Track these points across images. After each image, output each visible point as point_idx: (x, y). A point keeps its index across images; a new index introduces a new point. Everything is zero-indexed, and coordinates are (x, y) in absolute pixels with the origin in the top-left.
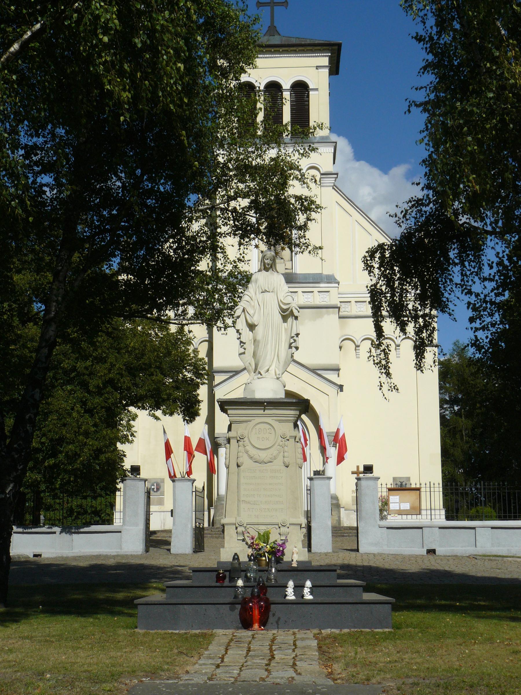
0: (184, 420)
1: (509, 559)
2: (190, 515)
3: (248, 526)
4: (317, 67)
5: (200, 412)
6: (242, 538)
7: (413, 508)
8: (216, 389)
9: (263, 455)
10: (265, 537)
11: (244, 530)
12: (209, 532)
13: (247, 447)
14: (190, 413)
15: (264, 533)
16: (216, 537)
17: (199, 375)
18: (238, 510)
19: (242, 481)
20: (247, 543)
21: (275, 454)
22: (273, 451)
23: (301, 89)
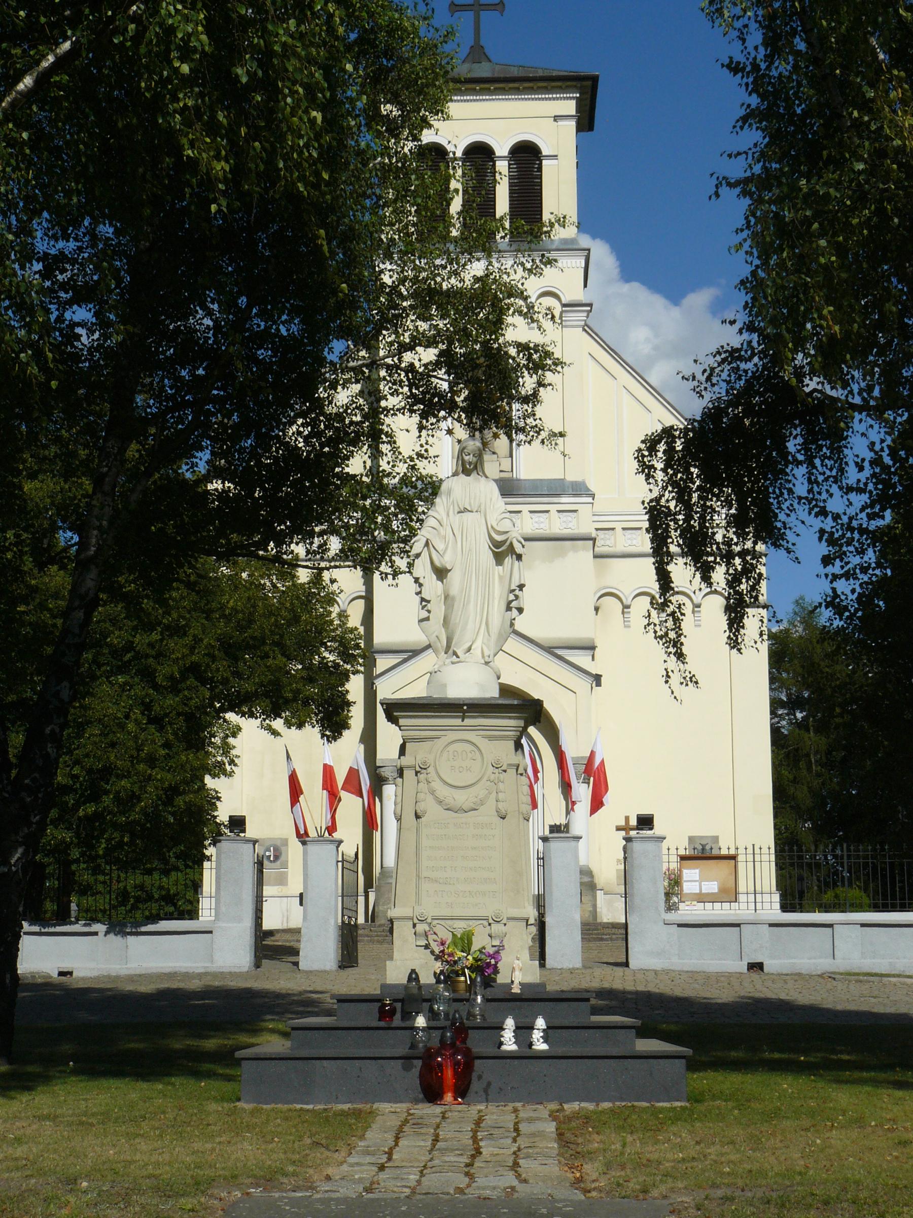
0: (323, 736)
1: (892, 979)
2: (333, 903)
3: (435, 922)
4: (556, 118)
5: (351, 722)
6: (424, 943)
7: (723, 890)
8: (378, 682)
9: (461, 798)
10: (465, 941)
11: (427, 929)
12: (366, 932)
13: (433, 784)
15: (463, 934)
16: (378, 941)
17: (348, 658)
18: (418, 894)
19: (425, 842)
20: (432, 952)
21: (481, 796)
22: (479, 791)
23: (527, 156)
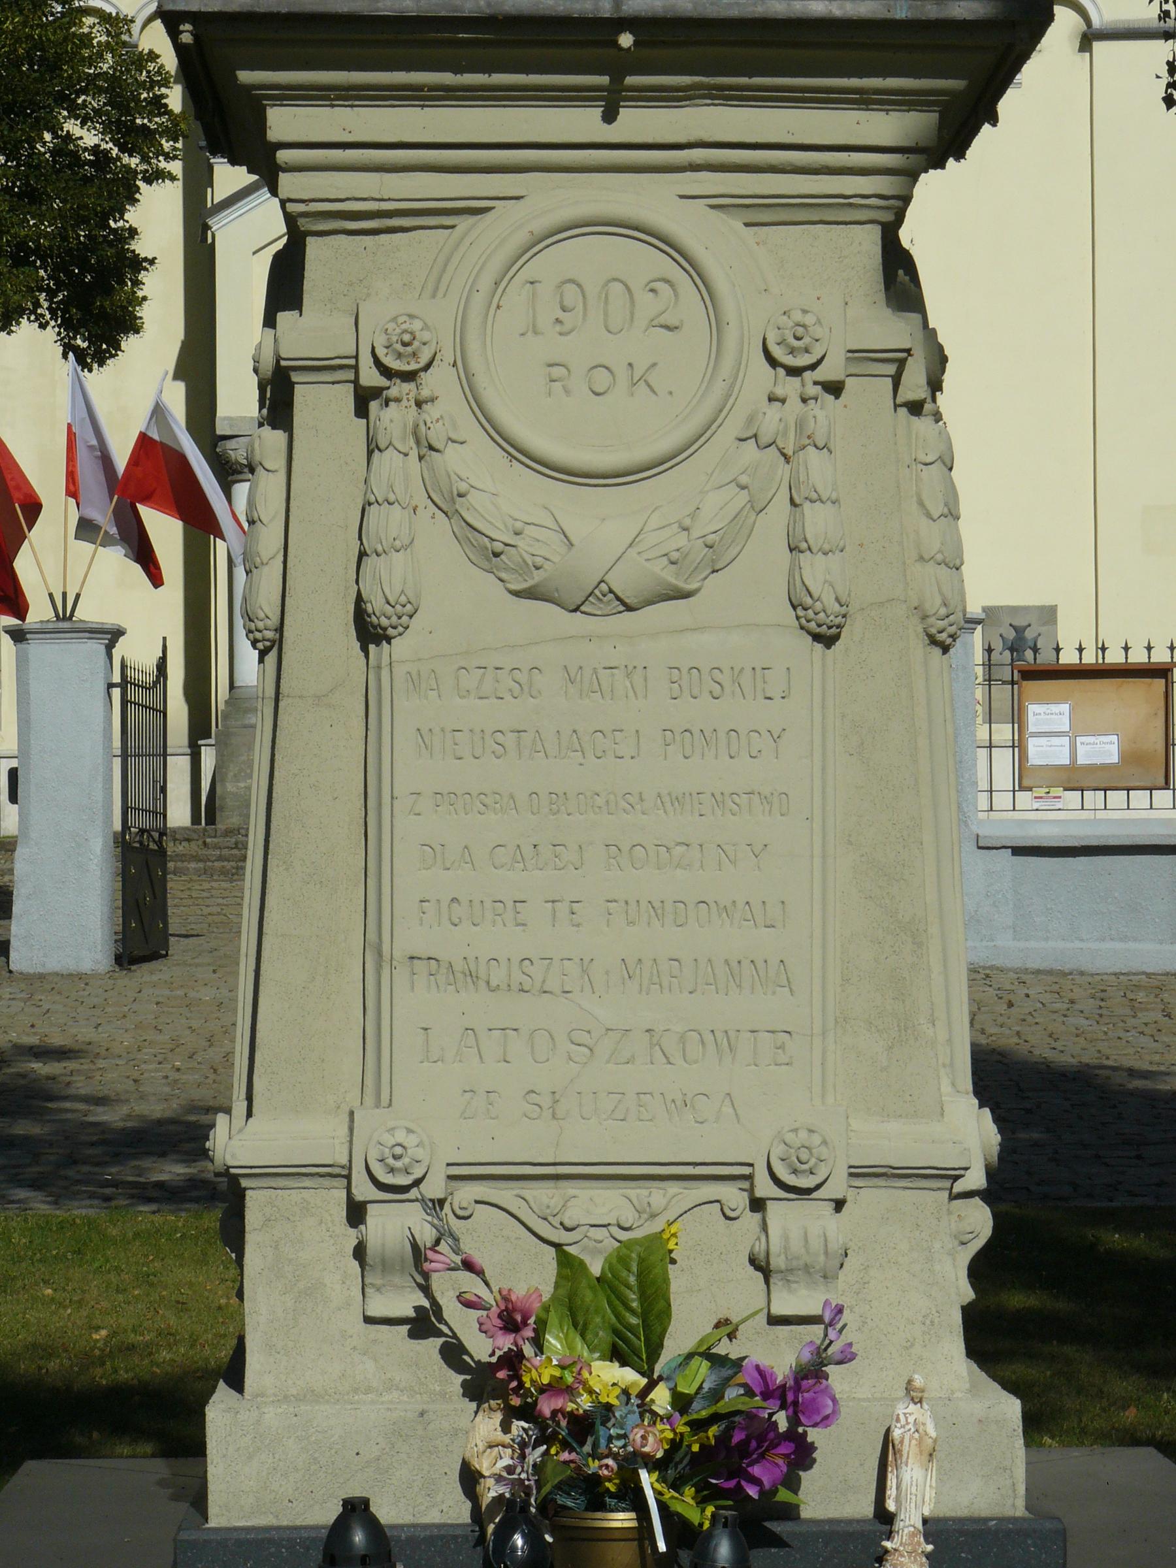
0: (68, 348)
2: (99, 795)
3: (466, 1194)
5: (146, 313)
6: (406, 1303)
7: (1131, 757)
8: (215, 223)
9: (606, 534)
10: (626, 1303)
11: (426, 1235)
12: (194, 848)
13: (452, 460)
14: (96, 320)
15: (619, 1259)
16: (224, 872)
17: (134, 139)
18: (372, 1042)
19: (409, 770)
20: (453, 1354)
21: (709, 522)
22: (701, 496)
